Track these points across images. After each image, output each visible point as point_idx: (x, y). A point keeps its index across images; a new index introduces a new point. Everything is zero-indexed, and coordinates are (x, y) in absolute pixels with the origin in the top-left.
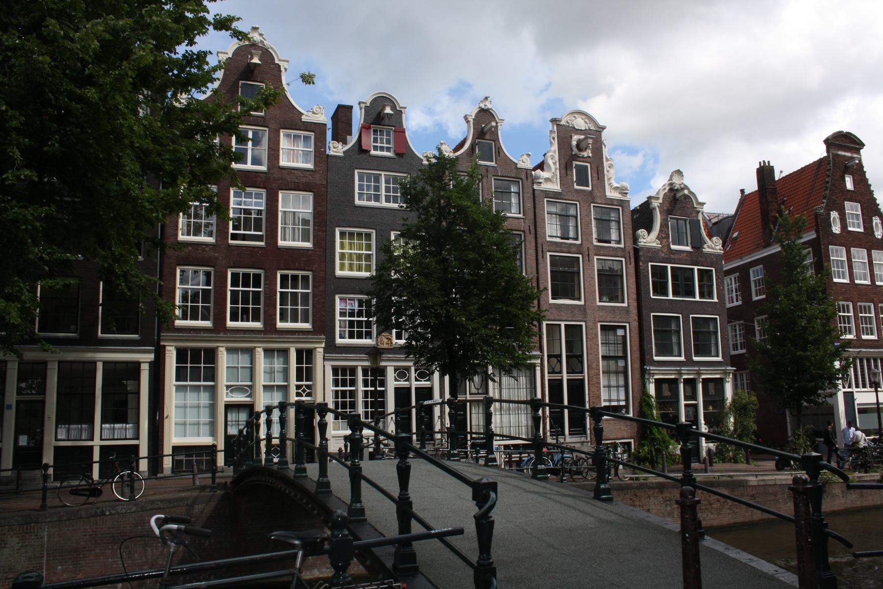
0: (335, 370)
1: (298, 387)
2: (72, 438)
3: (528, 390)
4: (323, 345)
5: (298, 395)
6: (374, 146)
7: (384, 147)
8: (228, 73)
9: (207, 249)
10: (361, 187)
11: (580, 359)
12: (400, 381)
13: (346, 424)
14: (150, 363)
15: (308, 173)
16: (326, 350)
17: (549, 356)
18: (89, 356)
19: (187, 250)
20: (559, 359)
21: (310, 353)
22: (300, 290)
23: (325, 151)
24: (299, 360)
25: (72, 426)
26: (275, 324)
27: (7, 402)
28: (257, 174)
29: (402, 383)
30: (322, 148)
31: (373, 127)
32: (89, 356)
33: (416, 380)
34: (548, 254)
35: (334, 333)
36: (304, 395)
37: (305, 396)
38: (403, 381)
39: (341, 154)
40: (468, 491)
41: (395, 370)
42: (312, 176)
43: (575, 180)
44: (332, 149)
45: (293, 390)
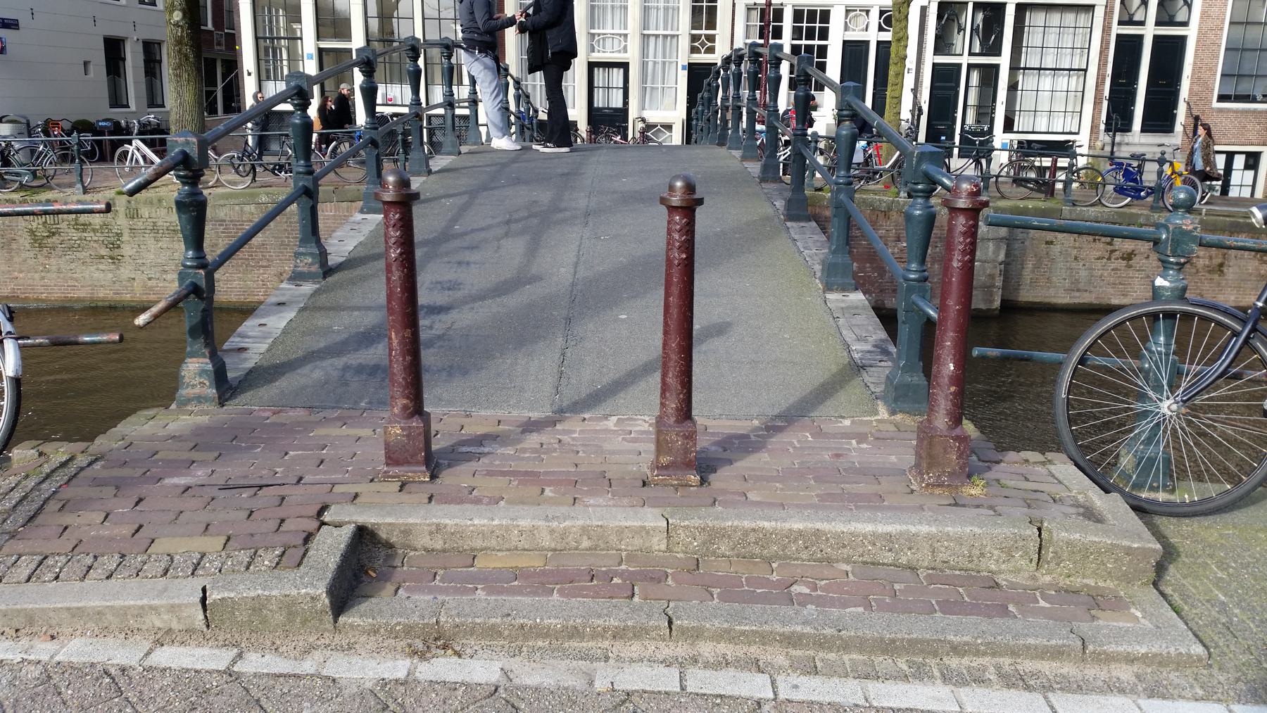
36: (703, 51)
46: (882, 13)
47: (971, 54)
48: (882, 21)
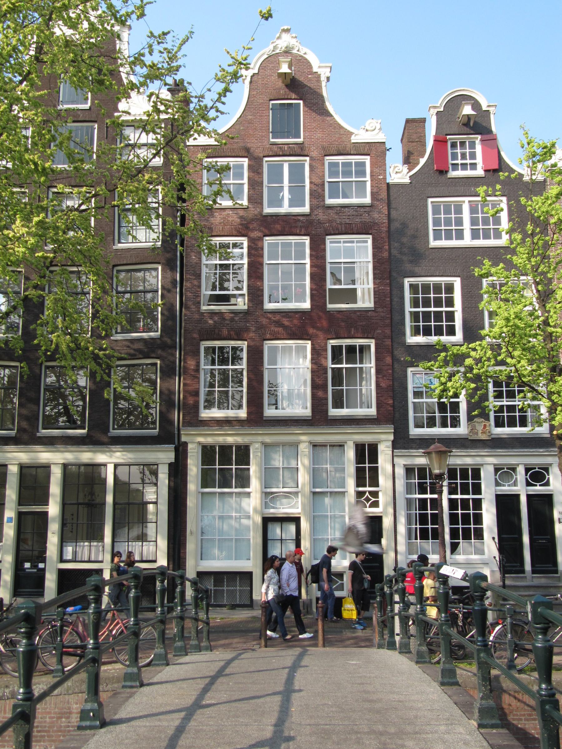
0: (409, 471)
2: (80, 559)
3: (30, 553)
6: (453, 164)
7: (466, 164)
8: (255, 93)
9: (236, 319)
10: (437, 222)
12: (536, 485)
13: (438, 544)
14: (170, 465)
15: (362, 210)
16: (395, 445)
18: (101, 458)
21: (373, 449)
22: (344, 366)
23: (385, 179)
25: (92, 544)
26: (327, 411)
28: (295, 218)
29: (538, 488)
30: (380, 174)
31: (450, 139)
32: (101, 458)
33: (515, 484)
35: (407, 420)
36: (368, 505)
37: (370, 507)
38: (540, 485)
39: (407, 180)
40: (108, 720)
41: (527, 470)
42: (368, 213)
43: (271, 130)
44: (393, 175)
48: (497, 477)
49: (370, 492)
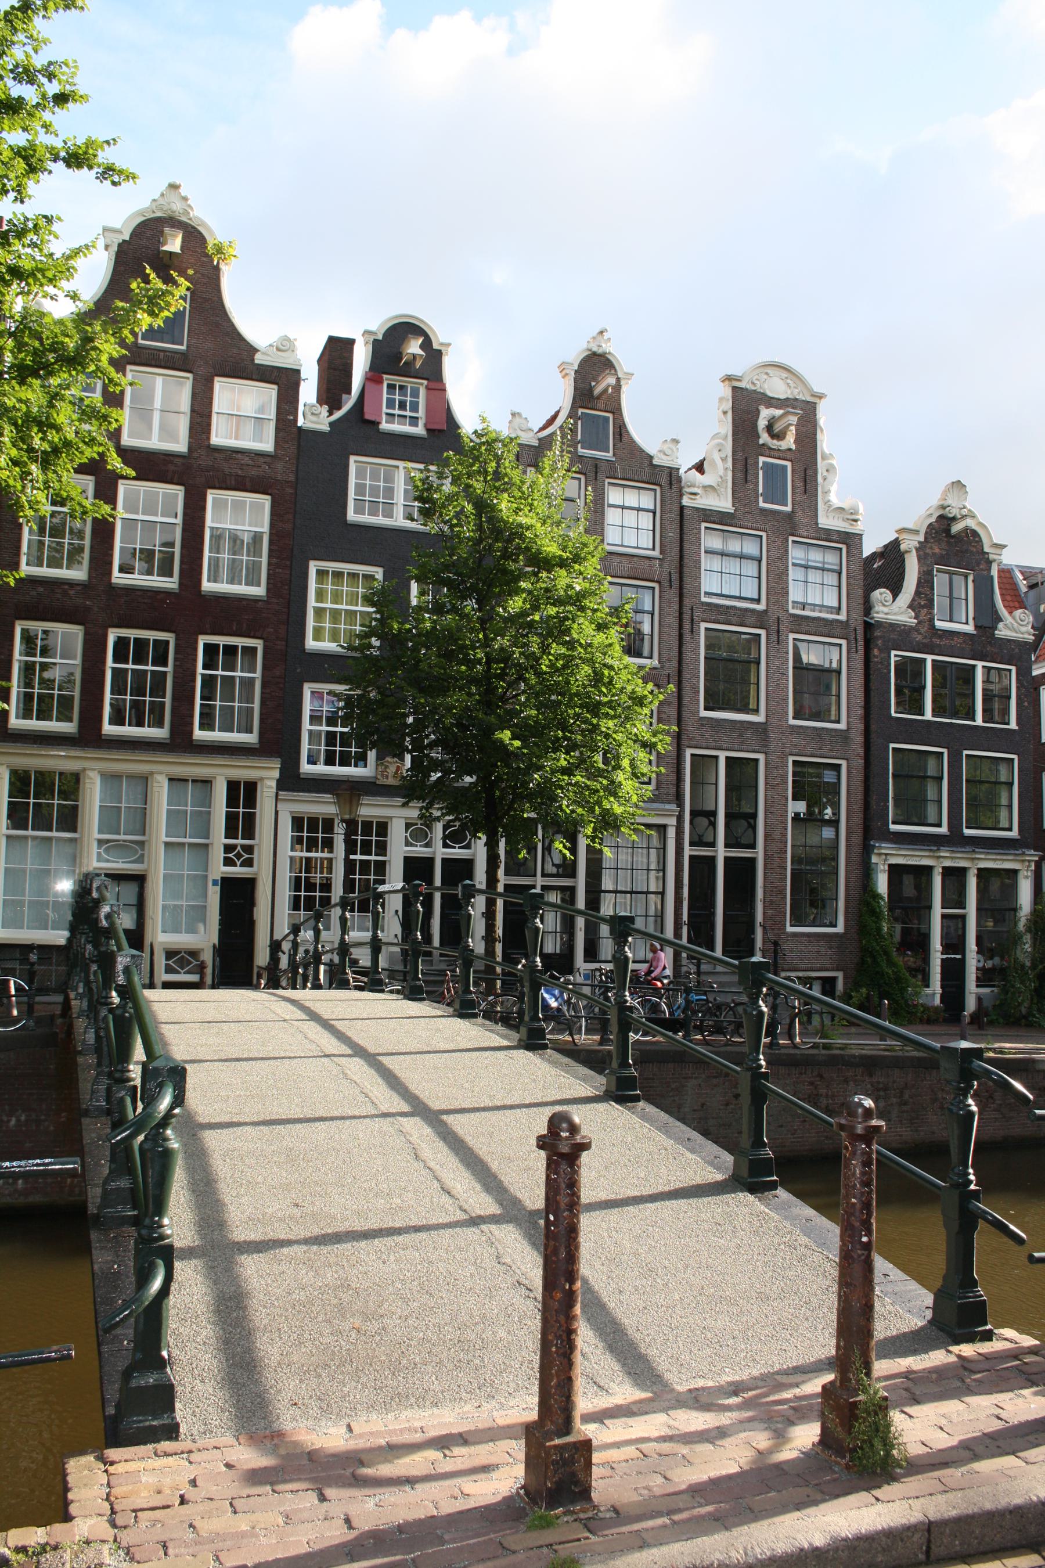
1: (228, 849)
4: (276, 774)
5: (228, 862)
11: (752, 821)
17: (694, 814)
19: (34, 593)
20: (752, 821)
21: (251, 788)
24: (232, 800)
27: (218, 888)
33: (445, 846)
34: (703, 625)
36: (238, 863)
45: (218, 854)
46: (408, 826)
47: (544, 875)
49: (243, 847)
